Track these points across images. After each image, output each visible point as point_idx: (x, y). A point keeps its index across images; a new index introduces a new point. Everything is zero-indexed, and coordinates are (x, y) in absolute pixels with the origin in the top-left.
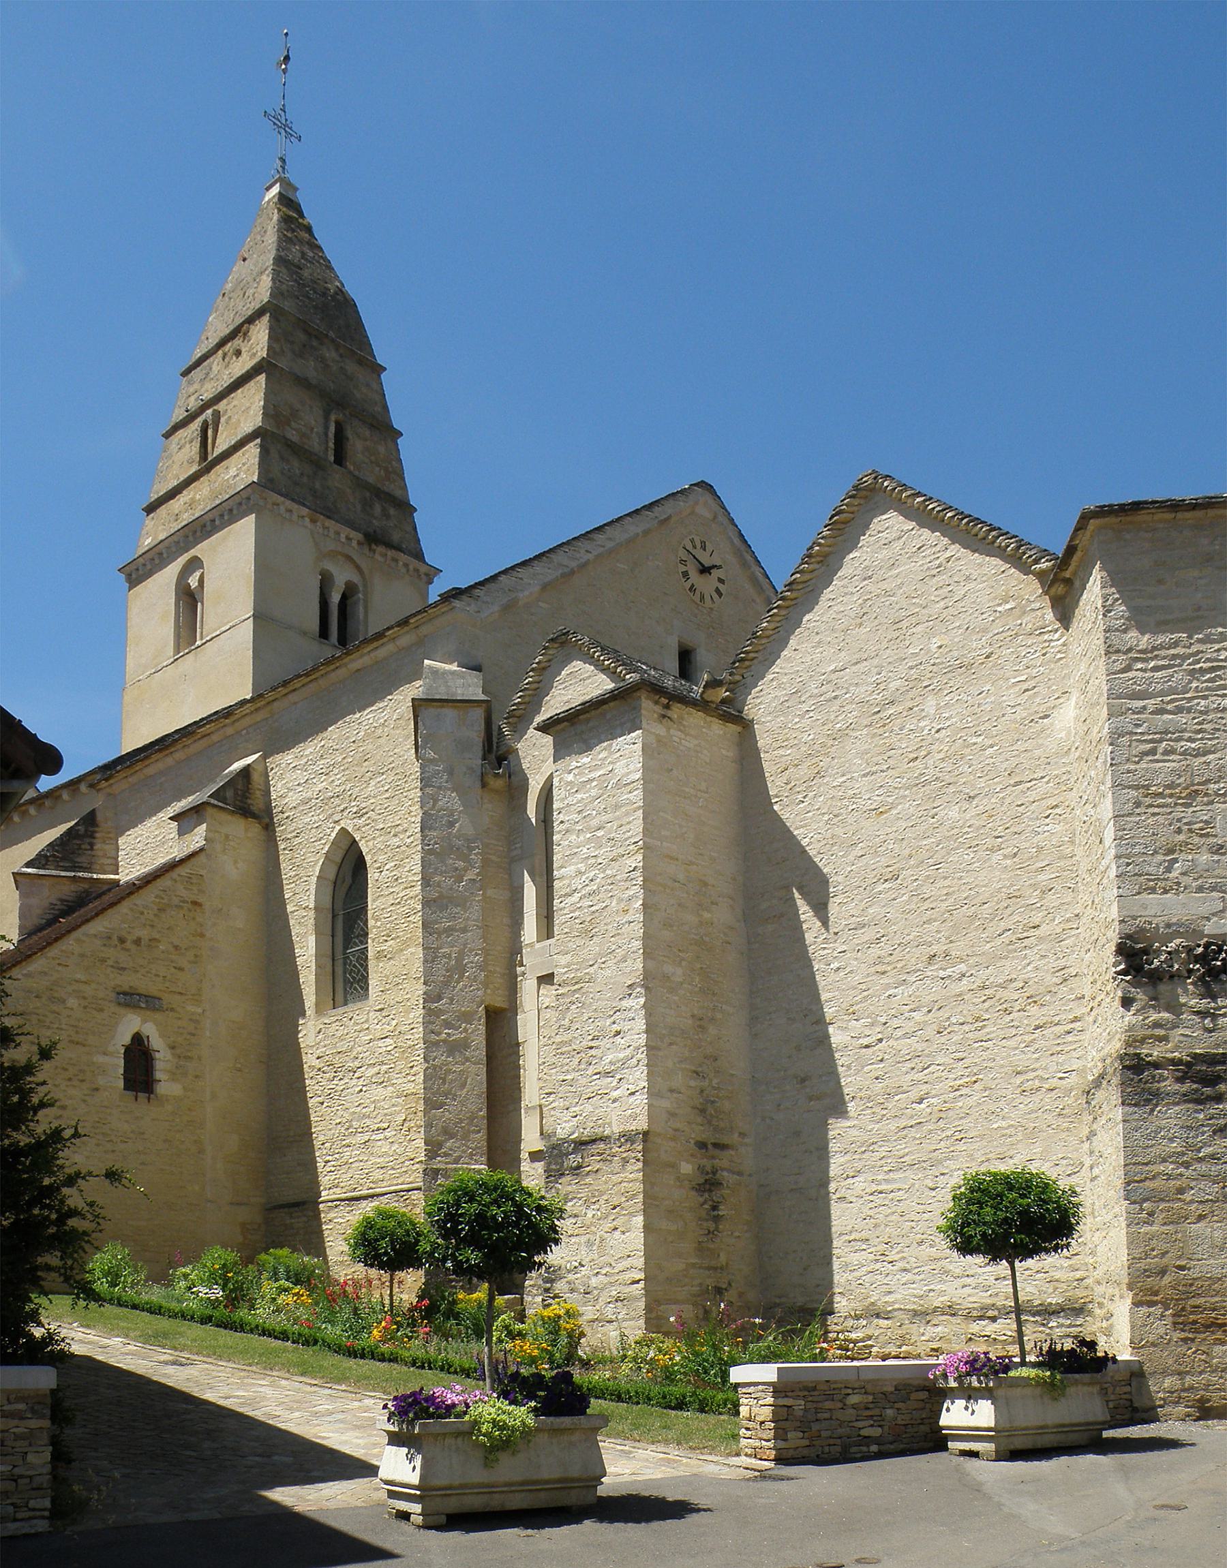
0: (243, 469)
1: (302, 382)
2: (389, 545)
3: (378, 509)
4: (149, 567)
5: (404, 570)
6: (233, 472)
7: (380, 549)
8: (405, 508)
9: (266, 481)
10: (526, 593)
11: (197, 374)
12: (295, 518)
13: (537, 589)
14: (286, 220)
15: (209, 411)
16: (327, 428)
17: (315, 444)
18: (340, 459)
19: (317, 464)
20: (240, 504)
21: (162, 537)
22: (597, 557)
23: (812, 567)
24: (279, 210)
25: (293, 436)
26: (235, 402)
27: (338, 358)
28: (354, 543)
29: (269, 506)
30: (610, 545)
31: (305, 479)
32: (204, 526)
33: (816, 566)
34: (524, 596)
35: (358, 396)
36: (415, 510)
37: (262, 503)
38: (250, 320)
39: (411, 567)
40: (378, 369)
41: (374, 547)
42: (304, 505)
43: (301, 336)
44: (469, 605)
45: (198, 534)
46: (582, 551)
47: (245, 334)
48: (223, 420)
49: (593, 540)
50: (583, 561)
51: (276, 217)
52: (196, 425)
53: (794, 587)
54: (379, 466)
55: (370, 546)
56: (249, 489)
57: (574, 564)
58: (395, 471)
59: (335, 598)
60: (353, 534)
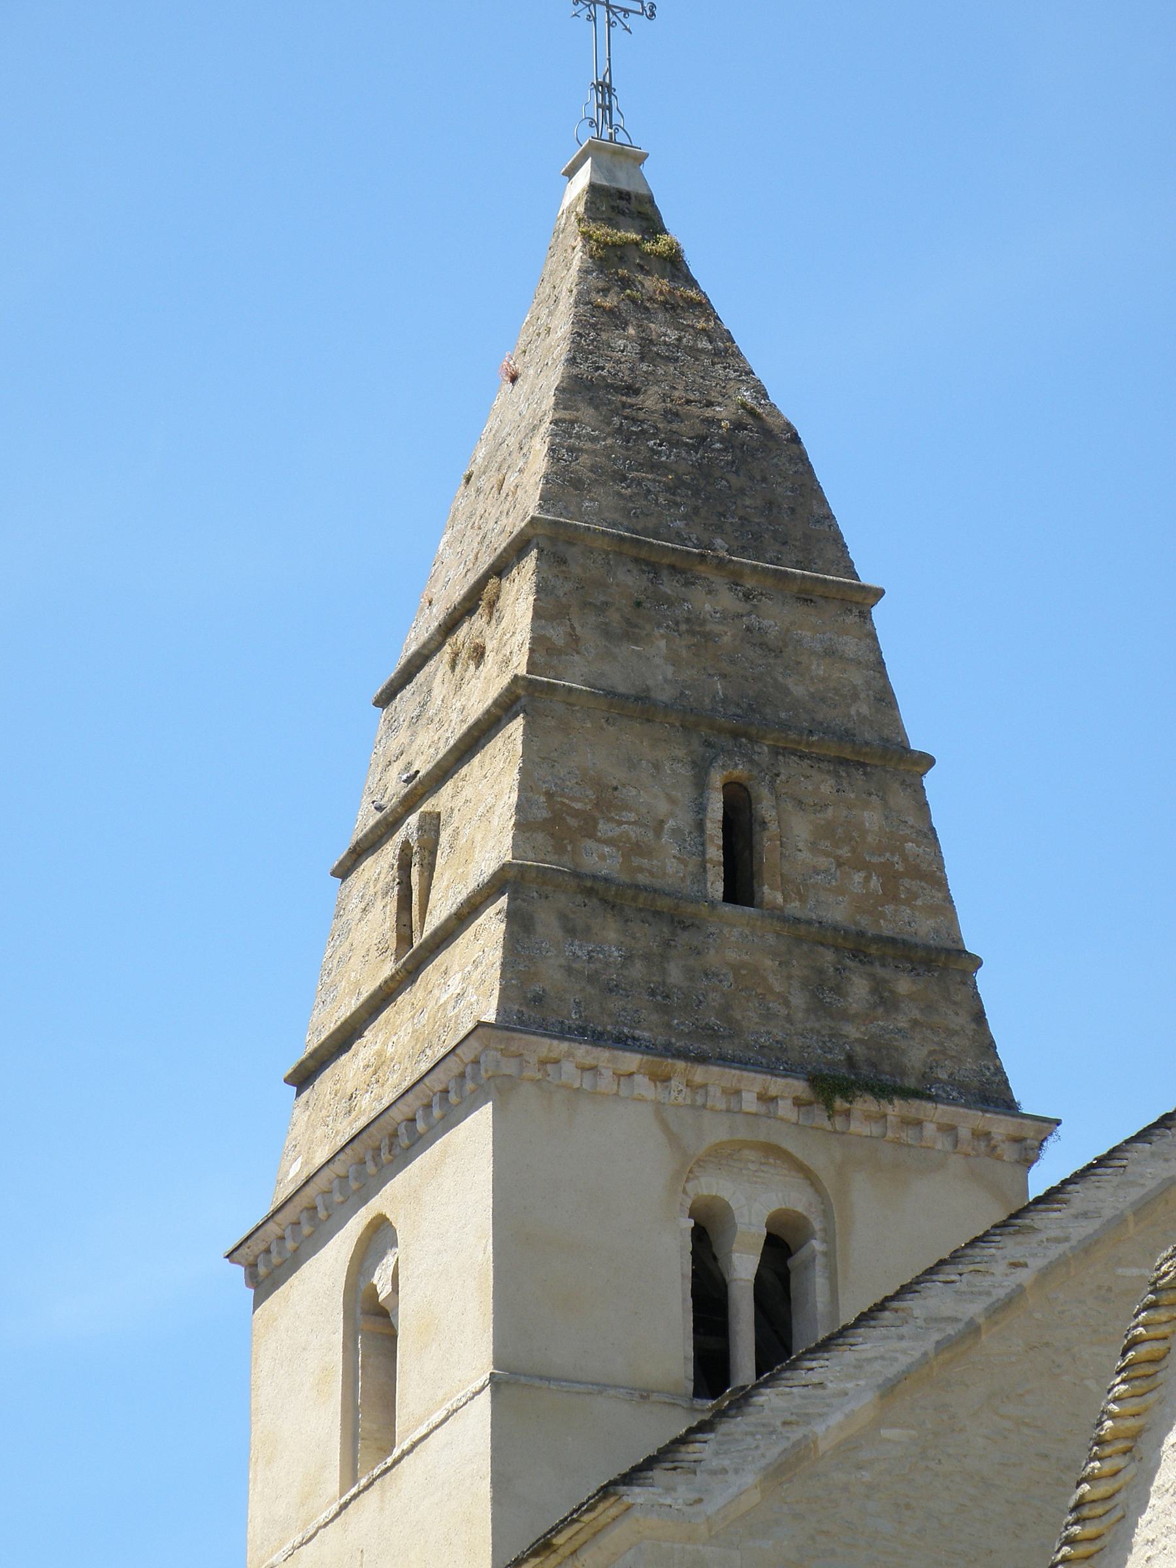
0: (469, 982)
1: (635, 706)
2: (885, 1091)
3: (859, 989)
4: (290, 1245)
5: (943, 1143)
6: (455, 984)
7: (865, 1104)
8: (949, 964)
9: (528, 1007)
10: (836, 1418)
11: (407, 700)
12: (606, 1083)
13: (870, 1397)
14: (608, 261)
15: (413, 820)
16: (701, 808)
17: (669, 865)
18: (740, 887)
19: (672, 916)
20: (462, 1075)
21: (320, 1157)
22: (1045, 1274)
23: (1109, 1466)
24: (587, 237)
25: (600, 860)
26: (468, 792)
27: (741, 607)
28: (785, 1109)
29: (531, 1072)
30: (1087, 1228)
31: (637, 970)
32: (394, 1135)
33: (1119, 1462)
34: (827, 1430)
35: (798, 690)
36: (977, 962)
37: (510, 1067)
38: (500, 569)
39: (964, 1133)
40: (860, 600)
41: (839, 1103)
42: (622, 1042)
43: (630, 580)
44: (670, 1489)
45: (385, 1156)
46: (1000, 1268)
47: (492, 605)
48: (444, 837)
49: (1033, 1230)
50: (1001, 1293)
51: (578, 258)
52: (389, 853)
53: (1086, 1512)
54: (866, 867)
55: (829, 1105)
56: (472, 1041)
57: (974, 1309)
58: (918, 868)
59: (743, 1266)
60: (777, 1085)
